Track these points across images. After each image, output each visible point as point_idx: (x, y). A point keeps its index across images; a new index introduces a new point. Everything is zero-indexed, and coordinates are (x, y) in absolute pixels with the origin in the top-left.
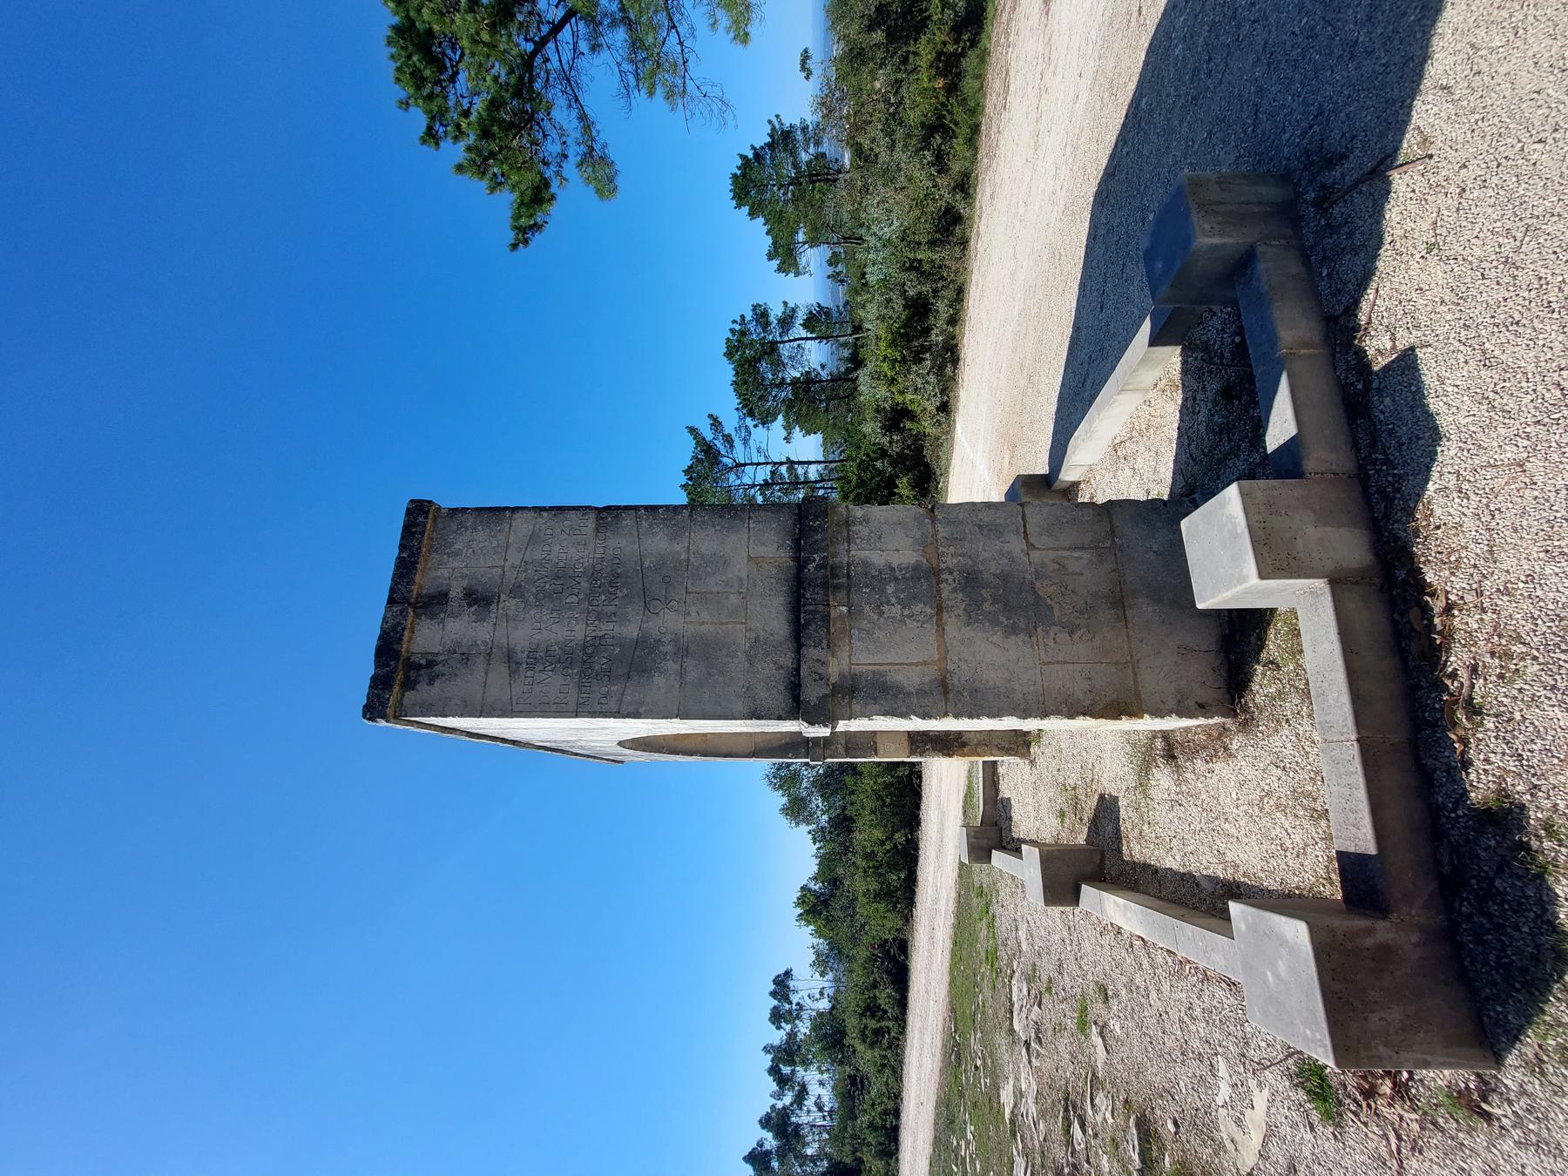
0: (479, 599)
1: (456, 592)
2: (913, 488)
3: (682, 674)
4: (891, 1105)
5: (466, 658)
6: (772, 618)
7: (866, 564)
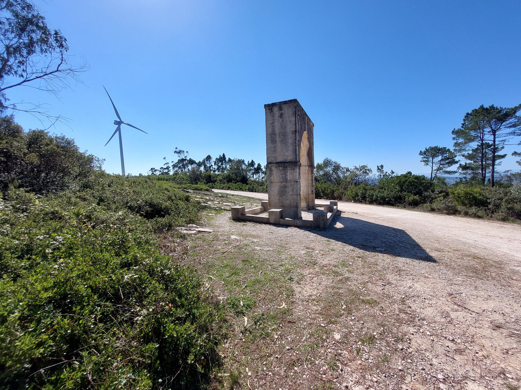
0: (281, 116)
1: (282, 112)
2: (413, 201)
3: (272, 148)
4: (257, 190)
5: (273, 116)
6: (280, 159)
7: (287, 172)
